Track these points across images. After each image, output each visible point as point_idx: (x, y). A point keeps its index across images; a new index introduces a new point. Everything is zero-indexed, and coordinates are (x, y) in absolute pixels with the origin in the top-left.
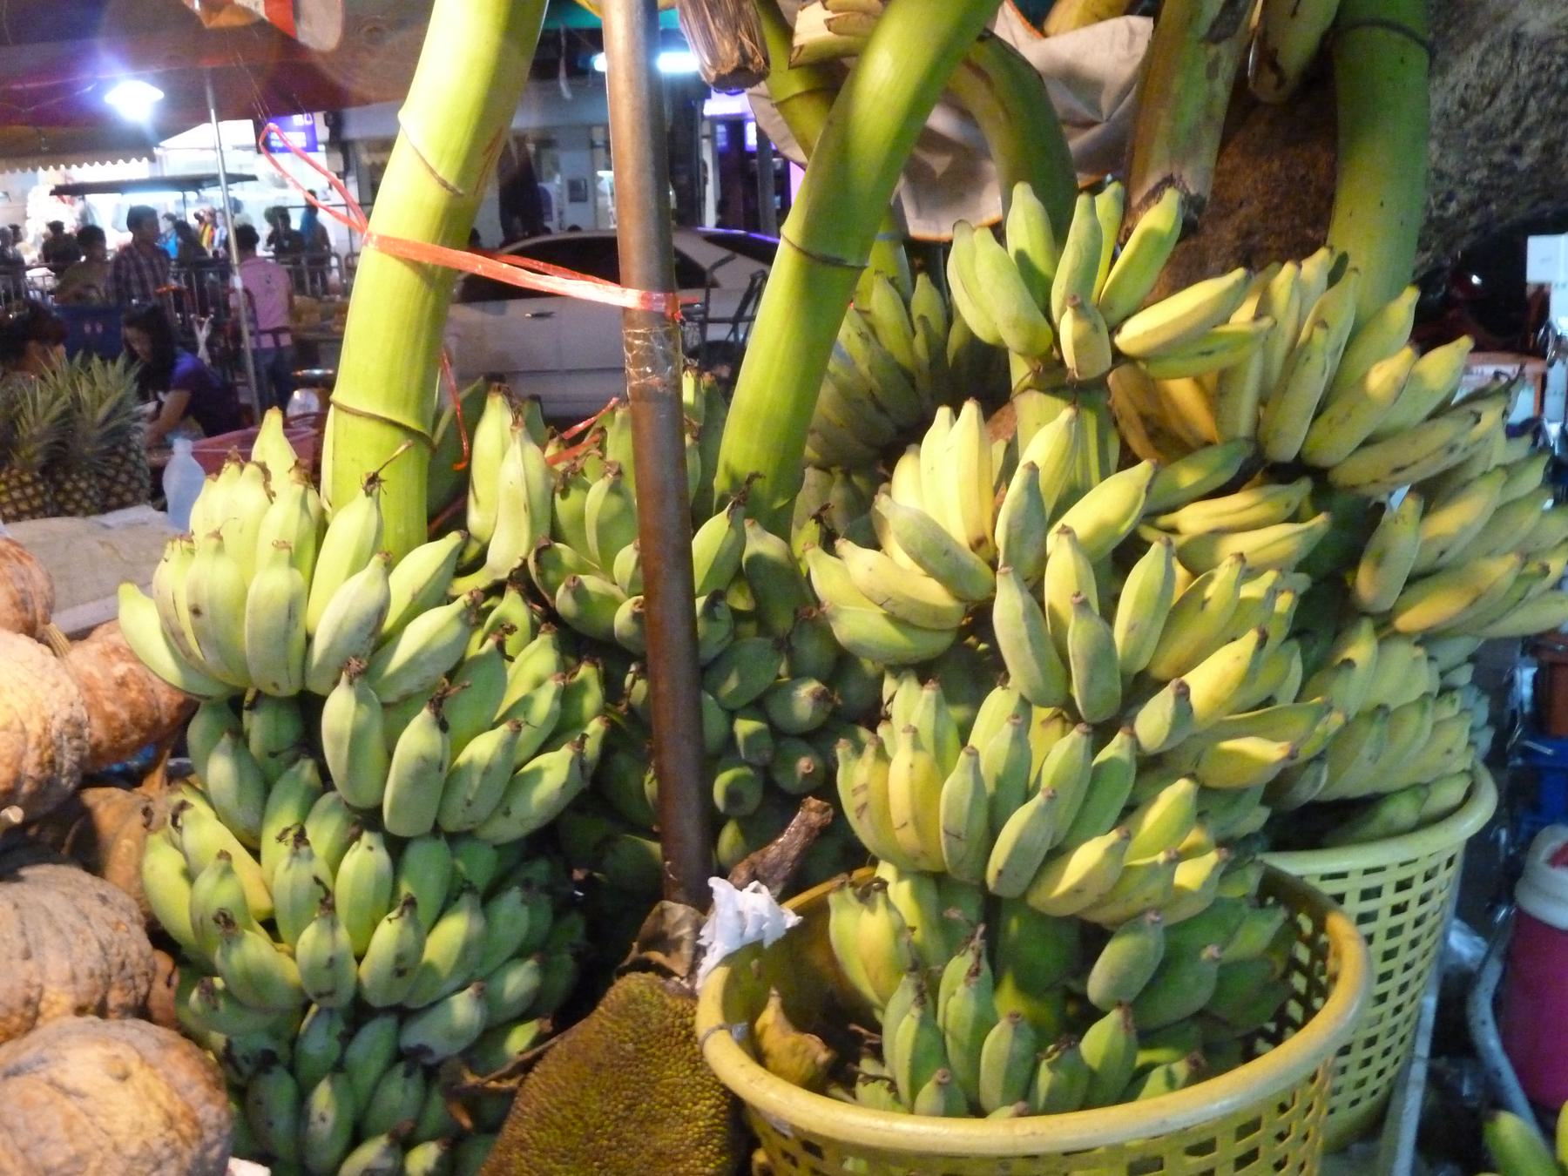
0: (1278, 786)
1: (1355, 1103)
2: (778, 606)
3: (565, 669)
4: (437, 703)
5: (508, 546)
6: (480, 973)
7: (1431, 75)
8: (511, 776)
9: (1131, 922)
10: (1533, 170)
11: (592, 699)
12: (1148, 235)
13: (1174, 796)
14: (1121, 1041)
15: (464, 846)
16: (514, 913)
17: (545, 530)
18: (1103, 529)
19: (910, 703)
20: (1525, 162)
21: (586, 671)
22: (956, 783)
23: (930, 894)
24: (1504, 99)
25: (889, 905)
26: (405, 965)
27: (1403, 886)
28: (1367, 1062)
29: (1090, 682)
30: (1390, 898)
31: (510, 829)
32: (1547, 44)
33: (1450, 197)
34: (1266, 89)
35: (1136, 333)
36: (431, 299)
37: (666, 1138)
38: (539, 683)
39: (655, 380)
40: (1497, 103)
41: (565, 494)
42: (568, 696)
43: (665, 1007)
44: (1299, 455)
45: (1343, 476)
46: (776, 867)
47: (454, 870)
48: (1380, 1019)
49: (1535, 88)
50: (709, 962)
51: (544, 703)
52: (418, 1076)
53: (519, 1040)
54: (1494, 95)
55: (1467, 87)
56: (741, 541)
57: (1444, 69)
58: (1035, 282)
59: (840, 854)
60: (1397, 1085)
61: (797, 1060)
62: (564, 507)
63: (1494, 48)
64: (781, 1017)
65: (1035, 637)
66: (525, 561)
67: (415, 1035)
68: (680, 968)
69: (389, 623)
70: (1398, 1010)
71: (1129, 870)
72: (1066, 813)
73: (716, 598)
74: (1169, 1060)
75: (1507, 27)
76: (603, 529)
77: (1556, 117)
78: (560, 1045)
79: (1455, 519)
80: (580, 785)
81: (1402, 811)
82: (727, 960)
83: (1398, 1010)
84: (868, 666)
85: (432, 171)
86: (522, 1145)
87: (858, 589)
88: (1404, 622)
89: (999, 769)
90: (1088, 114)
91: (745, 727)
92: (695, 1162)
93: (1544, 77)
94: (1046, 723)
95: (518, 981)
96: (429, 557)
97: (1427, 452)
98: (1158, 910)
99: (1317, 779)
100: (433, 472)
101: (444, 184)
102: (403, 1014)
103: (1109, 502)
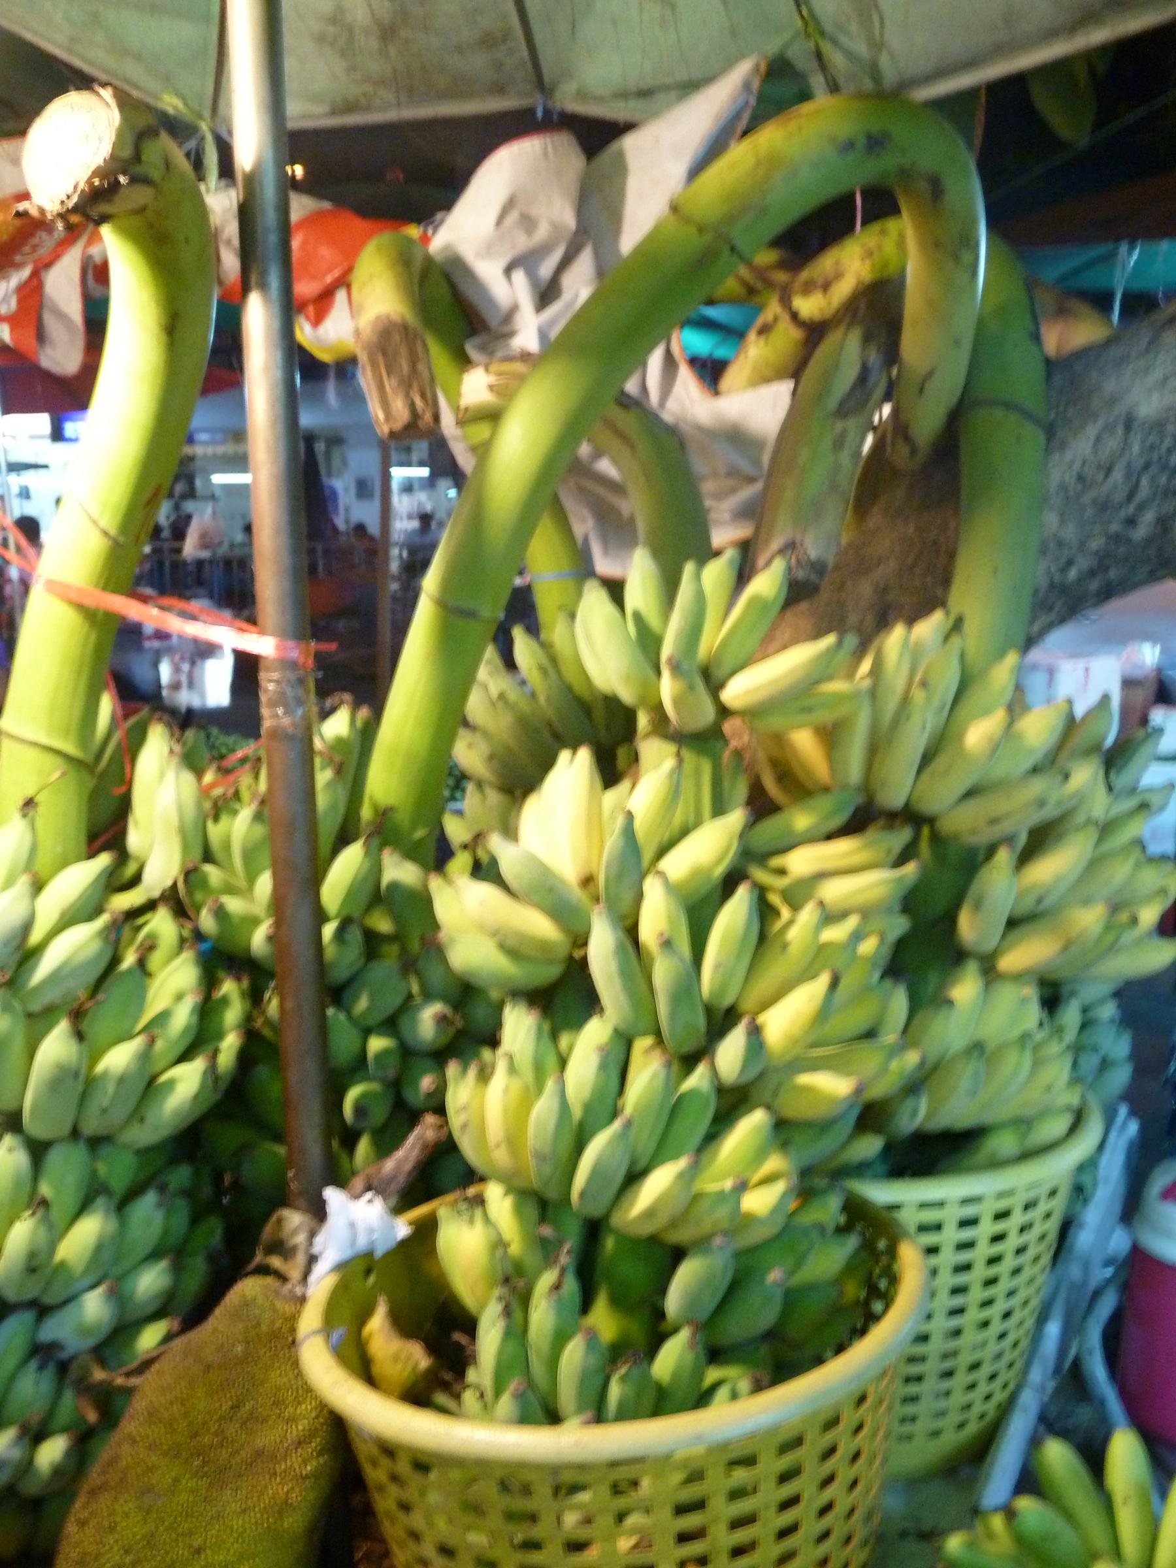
0: (870, 1115)
1: (961, 1426)
2: (400, 933)
3: (209, 982)
4: (77, 1016)
5: (161, 866)
6: (116, 1271)
7: (1048, 450)
8: (147, 1085)
9: (702, 1244)
10: (1148, 541)
11: (233, 1015)
12: (754, 601)
13: (752, 1124)
14: (690, 1357)
15: (105, 1150)
16: (148, 1214)
17: (197, 854)
18: (698, 873)
19: (519, 1027)
20: (1140, 533)
21: (229, 987)
22: (544, 1108)
23: (533, 1212)
24: (1118, 475)
25: (487, 1219)
26: (36, 1263)
27: (1002, 1215)
28: (972, 1387)
29: (673, 1015)
30: (987, 1227)
31: (145, 1134)
32: (1158, 426)
33: (1070, 563)
34: (900, 455)
35: (738, 690)
36: (93, 637)
37: (267, 1438)
38: (179, 997)
39: (286, 721)
40: (1110, 480)
41: (216, 818)
42: (208, 1010)
43: (275, 1310)
44: (907, 805)
45: (947, 825)
46: (392, 1179)
47: (94, 1173)
48: (984, 1344)
49: (1146, 467)
50: (322, 1268)
51: (182, 1017)
52: (50, 1371)
53: (149, 1338)
54: (1109, 470)
55: (1084, 462)
56: (377, 869)
57: (1063, 446)
58: (648, 641)
59: (442, 1174)
60: (1006, 1410)
61: (399, 1366)
62: (215, 832)
63: (1109, 428)
64: (387, 1325)
65: (625, 974)
66: (175, 884)
67: (51, 1330)
68: (295, 1274)
69: (35, 937)
70: (1002, 1336)
71: (697, 1197)
72: (646, 1143)
73: (345, 924)
74: (736, 1375)
75: (1120, 409)
76: (249, 855)
77: (1169, 493)
78: (178, 1343)
79: (1051, 868)
80: (213, 1098)
81: (1004, 1143)
82: (340, 1267)
83: (1002, 1336)
84: (494, 994)
85: (94, 522)
86: (133, 1441)
87: (472, 921)
88: (1010, 962)
89: (586, 1094)
90: (746, 467)
91: (377, 1044)
92: (295, 1460)
93: (1155, 457)
94: (648, 1051)
95: (150, 1281)
96: (84, 874)
97: (1019, 809)
98: (725, 1233)
99: (915, 1113)
100: (94, 798)
101: (106, 533)
102: (42, 1310)
103: (709, 845)
